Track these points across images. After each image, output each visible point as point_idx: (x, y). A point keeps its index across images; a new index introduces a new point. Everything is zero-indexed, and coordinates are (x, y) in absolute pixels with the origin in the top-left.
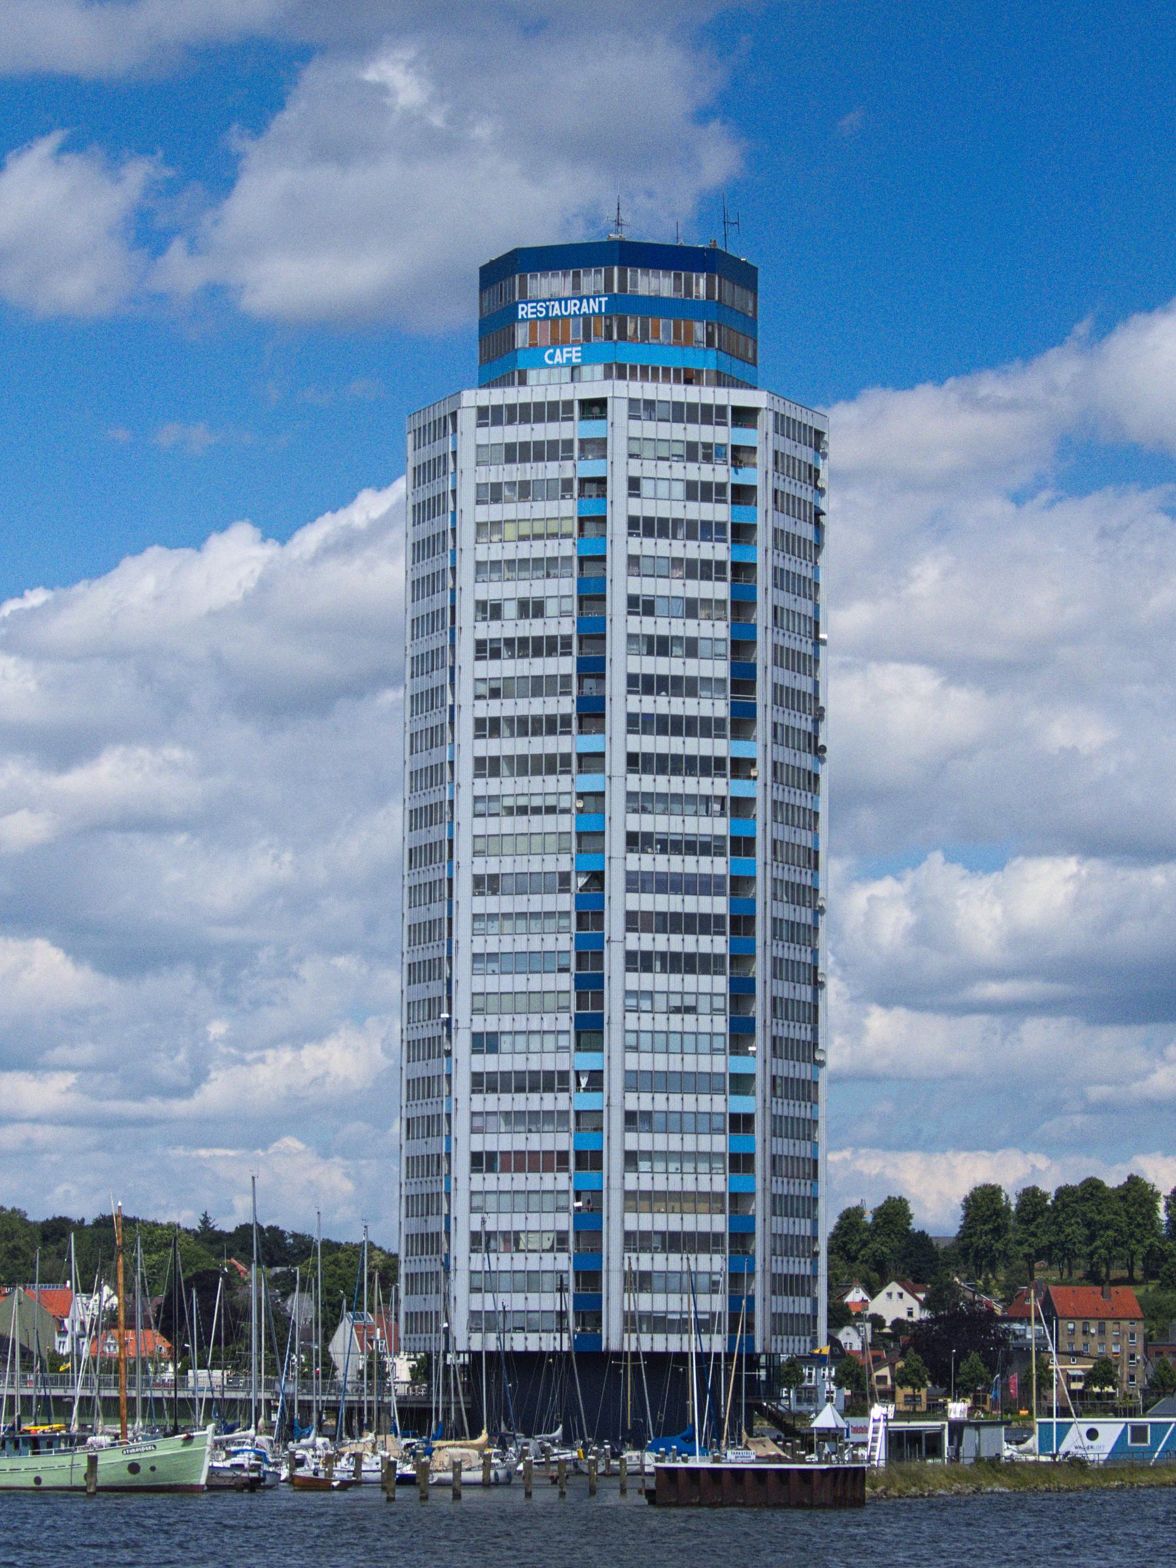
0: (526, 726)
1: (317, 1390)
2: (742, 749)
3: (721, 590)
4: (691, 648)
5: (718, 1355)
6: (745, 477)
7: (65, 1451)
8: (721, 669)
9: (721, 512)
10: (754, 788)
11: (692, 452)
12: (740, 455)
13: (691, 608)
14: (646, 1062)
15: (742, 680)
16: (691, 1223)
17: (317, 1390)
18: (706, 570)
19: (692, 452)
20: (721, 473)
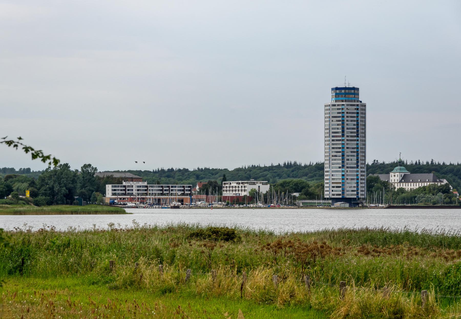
0: (351, 136)
1: (115, 190)
2: (343, 138)
3: (341, 123)
4: (338, 129)
5: (112, 187)
6: (343, 111)
7: (302, 207)
8: (341, 131)
9: (340, 115)
10: (359, 142)
11: (338, 109)
12: (342, 109)
13: (338, 125)
14: (334, 170)
15: (343, 131)
16: (338, 185)
17: (115, 190)
18: (339, 121)
19: (338, 109)
20: (340, 111)
